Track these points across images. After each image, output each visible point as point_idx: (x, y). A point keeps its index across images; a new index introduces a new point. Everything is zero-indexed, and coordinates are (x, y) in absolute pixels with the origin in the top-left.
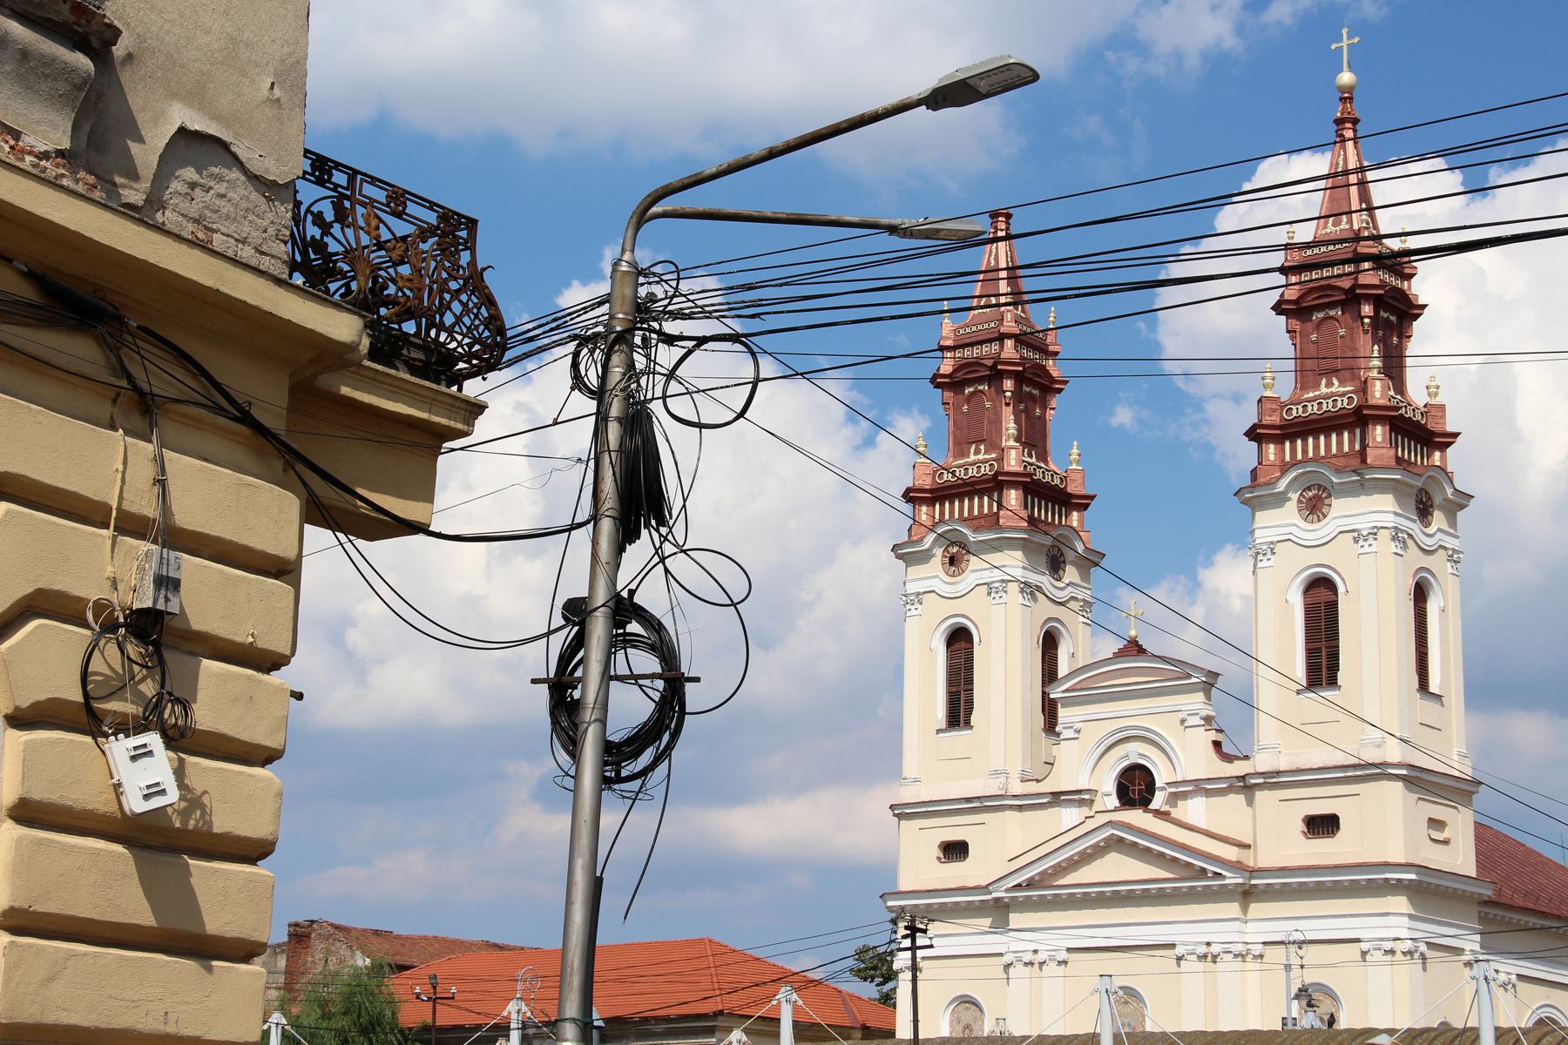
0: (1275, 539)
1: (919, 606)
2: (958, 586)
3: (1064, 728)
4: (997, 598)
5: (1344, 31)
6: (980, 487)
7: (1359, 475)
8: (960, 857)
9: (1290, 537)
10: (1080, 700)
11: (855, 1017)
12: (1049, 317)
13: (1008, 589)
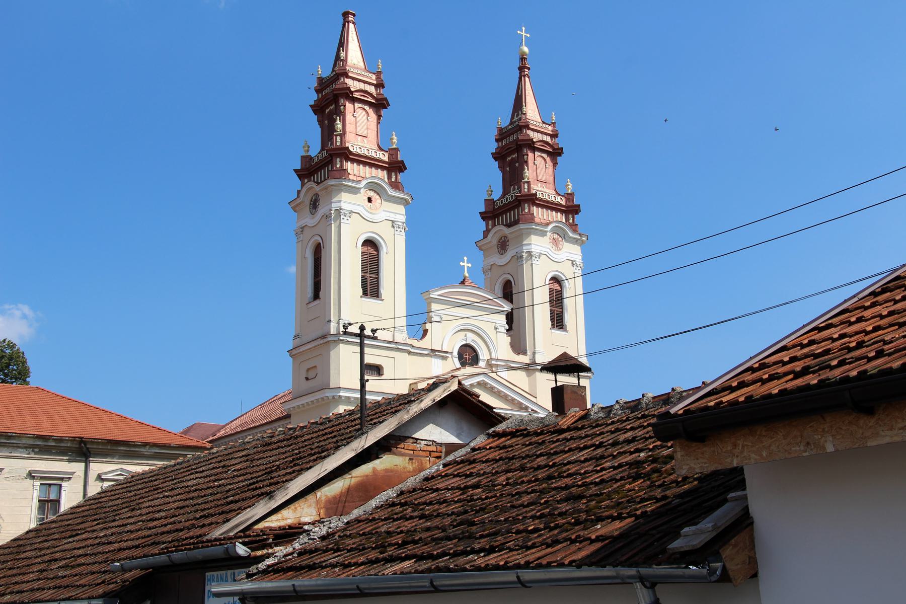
0: (543, 253)
1: (349, 218)
2: (375, 216)
3: (435, 315)
4: (399, 231)
5: (519, 32)
6: (538, 202)
7: (581, 236)
8: (369, 373)
9: (547, 253)
10: (443, 302)
11: (600, 519)
12: (501, 118)
13: (541, 258)
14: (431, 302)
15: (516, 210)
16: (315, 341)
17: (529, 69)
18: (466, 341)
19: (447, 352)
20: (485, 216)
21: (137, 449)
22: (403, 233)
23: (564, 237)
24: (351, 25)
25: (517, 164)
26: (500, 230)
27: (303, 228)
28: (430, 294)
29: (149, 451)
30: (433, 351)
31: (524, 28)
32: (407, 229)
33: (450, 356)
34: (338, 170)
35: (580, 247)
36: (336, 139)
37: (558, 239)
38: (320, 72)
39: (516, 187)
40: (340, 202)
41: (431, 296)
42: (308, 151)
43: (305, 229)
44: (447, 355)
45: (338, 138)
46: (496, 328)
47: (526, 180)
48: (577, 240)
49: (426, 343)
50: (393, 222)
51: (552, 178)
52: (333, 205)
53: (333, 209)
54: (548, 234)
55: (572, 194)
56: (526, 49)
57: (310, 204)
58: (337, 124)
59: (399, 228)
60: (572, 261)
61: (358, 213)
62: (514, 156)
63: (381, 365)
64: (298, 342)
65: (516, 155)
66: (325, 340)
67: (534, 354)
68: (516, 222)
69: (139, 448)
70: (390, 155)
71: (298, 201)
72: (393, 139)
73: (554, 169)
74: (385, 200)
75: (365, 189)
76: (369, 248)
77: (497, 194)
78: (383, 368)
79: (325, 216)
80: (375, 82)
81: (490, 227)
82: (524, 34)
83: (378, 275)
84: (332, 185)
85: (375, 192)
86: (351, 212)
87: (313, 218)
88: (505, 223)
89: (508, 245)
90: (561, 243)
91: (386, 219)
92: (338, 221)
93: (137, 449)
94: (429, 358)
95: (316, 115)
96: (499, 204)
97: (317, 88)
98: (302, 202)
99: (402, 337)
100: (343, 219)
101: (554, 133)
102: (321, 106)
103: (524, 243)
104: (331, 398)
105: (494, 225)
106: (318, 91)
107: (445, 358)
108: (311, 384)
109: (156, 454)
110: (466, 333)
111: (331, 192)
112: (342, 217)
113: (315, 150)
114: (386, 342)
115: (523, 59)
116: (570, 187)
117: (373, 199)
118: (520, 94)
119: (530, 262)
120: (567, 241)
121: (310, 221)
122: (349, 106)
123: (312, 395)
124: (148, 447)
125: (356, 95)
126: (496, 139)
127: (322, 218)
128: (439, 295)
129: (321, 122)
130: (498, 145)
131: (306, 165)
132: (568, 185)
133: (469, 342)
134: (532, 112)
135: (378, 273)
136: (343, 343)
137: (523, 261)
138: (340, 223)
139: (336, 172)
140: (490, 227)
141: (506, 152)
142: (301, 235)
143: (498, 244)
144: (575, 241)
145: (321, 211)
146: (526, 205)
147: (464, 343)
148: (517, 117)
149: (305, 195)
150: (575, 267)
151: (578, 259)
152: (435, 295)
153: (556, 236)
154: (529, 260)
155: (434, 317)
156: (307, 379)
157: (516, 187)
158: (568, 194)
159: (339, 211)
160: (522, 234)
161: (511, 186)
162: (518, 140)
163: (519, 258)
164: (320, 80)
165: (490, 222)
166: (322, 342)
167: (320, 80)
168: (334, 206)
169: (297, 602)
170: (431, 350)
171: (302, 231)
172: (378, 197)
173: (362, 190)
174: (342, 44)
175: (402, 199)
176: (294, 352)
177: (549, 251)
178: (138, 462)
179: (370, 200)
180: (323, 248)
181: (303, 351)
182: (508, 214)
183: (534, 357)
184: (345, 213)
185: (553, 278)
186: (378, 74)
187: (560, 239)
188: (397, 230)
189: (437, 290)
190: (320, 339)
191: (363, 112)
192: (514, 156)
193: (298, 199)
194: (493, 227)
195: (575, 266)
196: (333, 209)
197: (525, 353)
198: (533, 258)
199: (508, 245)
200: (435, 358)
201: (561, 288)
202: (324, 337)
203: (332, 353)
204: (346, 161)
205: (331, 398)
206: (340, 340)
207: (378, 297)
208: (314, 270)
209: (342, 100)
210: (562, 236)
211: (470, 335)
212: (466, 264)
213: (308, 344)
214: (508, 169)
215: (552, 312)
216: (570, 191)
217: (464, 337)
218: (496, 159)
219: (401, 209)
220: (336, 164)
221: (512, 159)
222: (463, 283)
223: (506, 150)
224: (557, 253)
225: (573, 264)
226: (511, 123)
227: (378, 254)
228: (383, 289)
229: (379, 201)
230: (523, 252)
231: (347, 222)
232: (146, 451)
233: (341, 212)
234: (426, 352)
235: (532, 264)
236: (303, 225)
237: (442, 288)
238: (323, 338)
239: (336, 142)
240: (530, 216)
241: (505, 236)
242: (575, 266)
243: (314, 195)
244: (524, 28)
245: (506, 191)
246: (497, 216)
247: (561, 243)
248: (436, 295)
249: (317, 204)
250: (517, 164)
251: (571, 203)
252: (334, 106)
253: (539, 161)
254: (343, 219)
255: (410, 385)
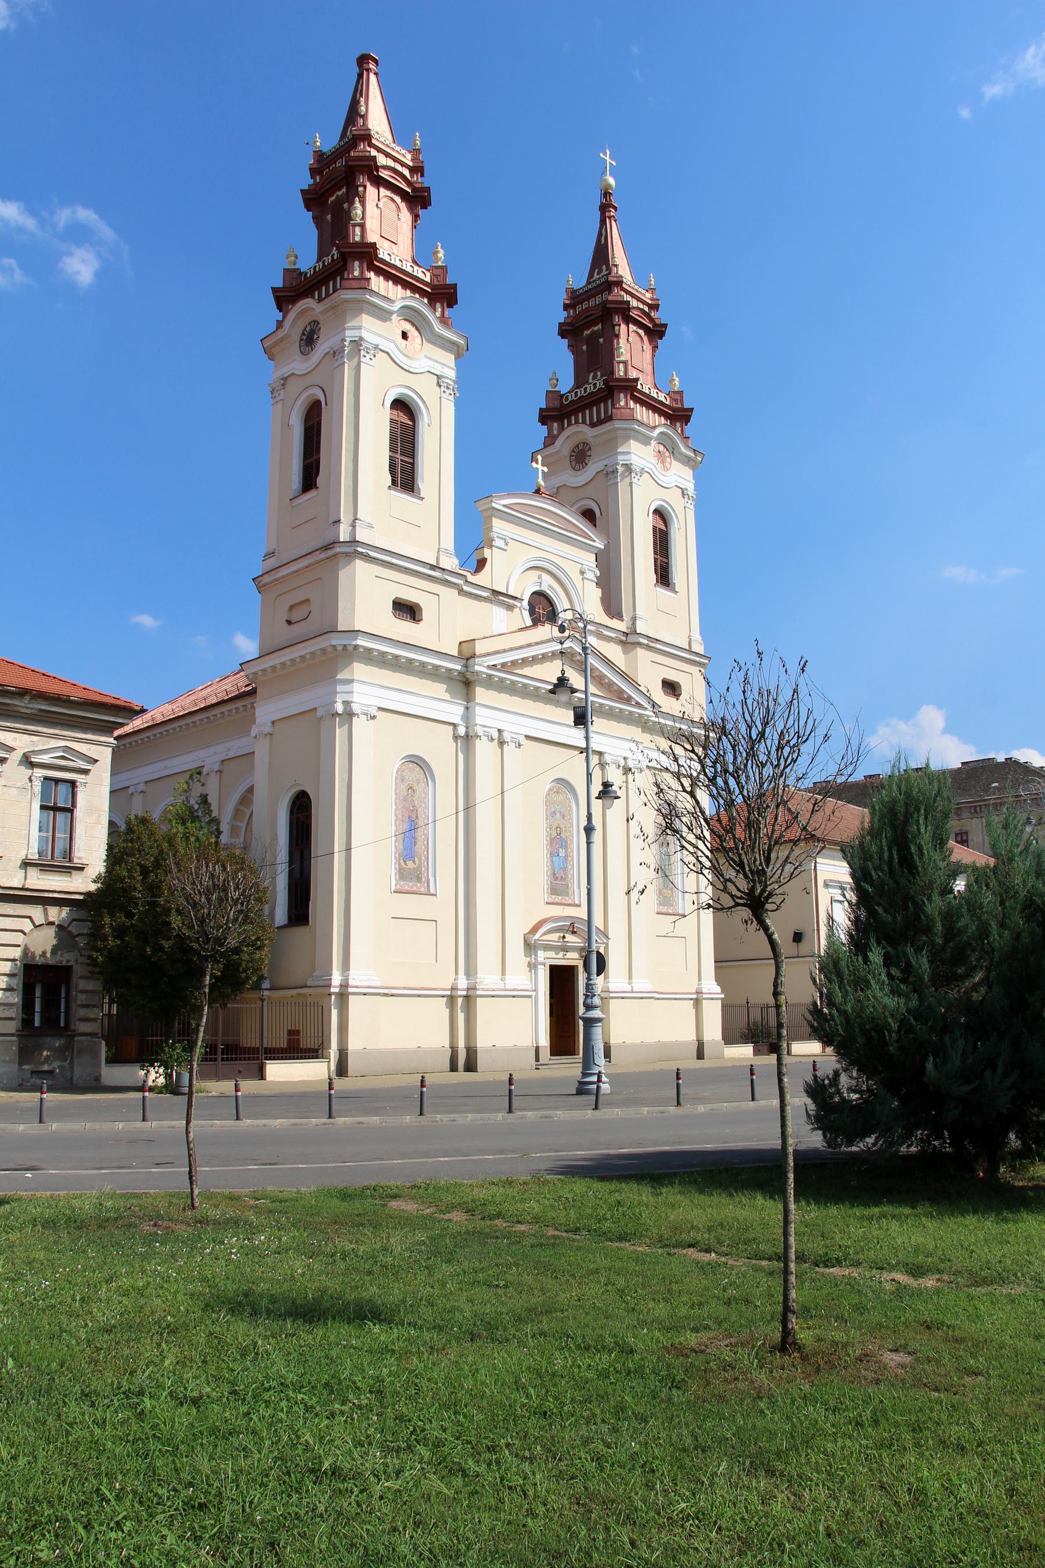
1: (372, 357)
7: (695, 454)
14: (491, 517)
15: (587, 412)
16: (308, 557)
17: (615, 209)
18: (540, 586)
19: (515, 598)
20: (544, 418)
21: (8, 701)
22: (452, 398)
23: (673, 451)
24: (372, 76)
25: (601, 340)
26: (578, 431)
27: (285, 379)
28: (492, 501)
29: (31, 706)
30: (495, 593)
31: (608, 152)
32: (458, 395)
33: (519, 605)
34: (355, 279)
35: (691, 471)
36: (354, 231)
37: (664, 454)
38: (318, 144)
39: (599, 373)
40: (360, 328)
41: (494, 505)
42: (295, 264)
43: (290, 381)
44: (516, 603)
45: (358, 230)
46: (582, 573)
47: (622, 358)
48: (689, 459)
49: (482, 578)
50: (439, 377)
51: (650, 367)
52: (348, 333)
53: (348, 339)
54: (653, 442)
55: (680, 393)
56: (611, 181)
57: (301, 340)
58: (355, 208)
59: (448, 388)
60: (681, 489)
61: (387, 353)
62: (596, 328)
63: (417, 605)
64: (272, 562)
65: (600, 326)
66: (330, 553)
67: (634, 619)
68: (609, 418)
69: (10, 698)
70: (434, 276)
71: (281, 334)
72: (438, 252)
73: (653, 356)
74: (428, 341)
75: (398, 316)
76: (401, 414)
77: (566, 383)
78: (420, 609)
79: (332, 352)
80: (411, 164)
81: (555, 432)
82: (607, 159)
83: (413, 458)
84: (347, 301)
85: (413, 324)
86: (376, 347)
87: (308, 359)
88: (588, 423)
89: (590, 456)
90: (668, 460)
91: (428, 372)
92: (356, 359)
93: (8, 701)
94: (486, 605)
95: (308, 210)
96: (572, 397)
97: (315, 166)
98: (286, 336)
99: (450, 562)
100: (365, 356)
101: (653, 302)
102: (321, 192)
103: (619, 450)
104: (340, 648)
105: (562, 429)
106: (313, 172)
107: (510, 608)
108: (298, 630)
109: (40, 713)
110: (540, 573)
111: (341, 314)
112: (362, 353)
113: (308, 261)
114: (429, 566)
115: (606, 194)
116: (677, 383)
117: (409, 335)
118: (603, 242)
119: (628, 480)
120: (676, 459)
121: (298, 365)
122: (371, 191)
123: (304, 644)
124: (27, 697)
125: (384, 174)
126: (564, 304)
127: (323, 357)
128: (504, 506)
129: (318, 220)
130: (569, 313)
131: (291, 284)
132: (674, 380)
133: (545, 588)
134: (622, 267)
135: (413, 455)
136: (360, 559)
137: (616, 477)
138: (359, 363)
139: (352, 282)
140: (555, 432)
141: (586, 321)
142: (282, 392)
143: (571, 456)
144: (687, 461)
145: (322, 347)
146: (622, 395)
147: (537, 588)
148: (598, 274)
149: (293, 325)
150: (686, 499)
151: (690, 487)
152: (499, 504)
153: (662, 448)
154: (627, 477)
155: (496, 539)
156: (289, 622)
157: (599, 373)
158: (675, 392)
159: (357, 343)
160: (616, 438)
161: (590, 372)
162: (605, 302)
163: (609, 474)
164: (319, 155)
165: (555, 425)
166: (323, 556)
167: (319, 155)
168: (350, 335)
169: (411, 1045)
170: (493, 590)
171: (283, 385)
172: (417, 334)
173: (394, 317)
174: (359, 91)
175: (454, 343)
176: (267, 579)
177: (652, 467)
178: (9, 724)
179: (405, 335)
180: (326, 404)
181: (283, 577)
182: (595, 409)
183: (634, 624)
184: (367, 348)
185: (657, 512)
186: (416, 152)
187: (667, 454)
188: (444, 392)
189: (502, 498)
190: (318, 552)
191: (393, 206)
192: (596, 328)
193: (279, 331)
194: (560, 433)
195: (686, 496)
196: (348, 339)
197: (619, 616)
198: (633, 475)
199: (590, 456)
200: (496, 605)
201: (666, 526)
202: (327, 547)
203: (343, 575)
204: (369, 270)
205: (340, 648)
206: (356, 552)
207: (413, 492)
208: (305, 447)
209: (361, 177)
210: (671, 450)
211: (546, 577)
212: (540, 467)
213: (295, 562)
214: (585, 348)
215: (656, 560)
216: (676, 389)
217: (536, 579)
218: (563, 333)
219: (450, 359)
220: (353, 270)
221: (593, 332)
222: (538, 491)
223: (583, 320)
224: (663, 473)
225: (683, 493)
226: (588, 283)
227: (414, 426)
228: (423, 481)
229: (418, 340)
230: (618, 464)
231: (370, 362)
232: (24, 705)
233: (361, 345)
234: (485, 594)
235: (631, 484)
236: (286, 375)
237: (510, 495)
238: (326, 550)
239: (354, 235)
240: (628, 411)
241: (584, 443)
242: (686, 496)
243: (310, 323)
244: (608, 152)
245: (580, 380)
246: (568, 415)
247: (668, 460)
248: (500, 504)
249: (315, 336)
250: (601, 340)
251: (679, 406)
252: (344, 190)
253: (633, 337)
254: (365, 356)
255: (460, 643)
